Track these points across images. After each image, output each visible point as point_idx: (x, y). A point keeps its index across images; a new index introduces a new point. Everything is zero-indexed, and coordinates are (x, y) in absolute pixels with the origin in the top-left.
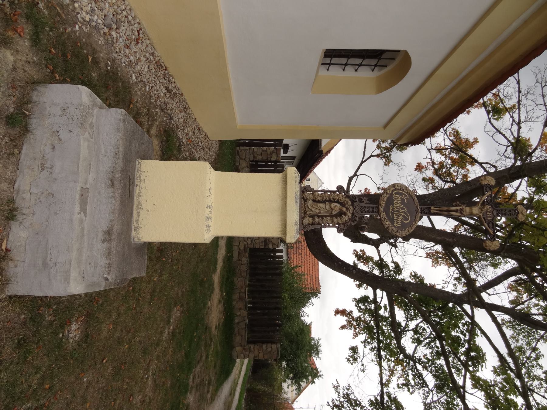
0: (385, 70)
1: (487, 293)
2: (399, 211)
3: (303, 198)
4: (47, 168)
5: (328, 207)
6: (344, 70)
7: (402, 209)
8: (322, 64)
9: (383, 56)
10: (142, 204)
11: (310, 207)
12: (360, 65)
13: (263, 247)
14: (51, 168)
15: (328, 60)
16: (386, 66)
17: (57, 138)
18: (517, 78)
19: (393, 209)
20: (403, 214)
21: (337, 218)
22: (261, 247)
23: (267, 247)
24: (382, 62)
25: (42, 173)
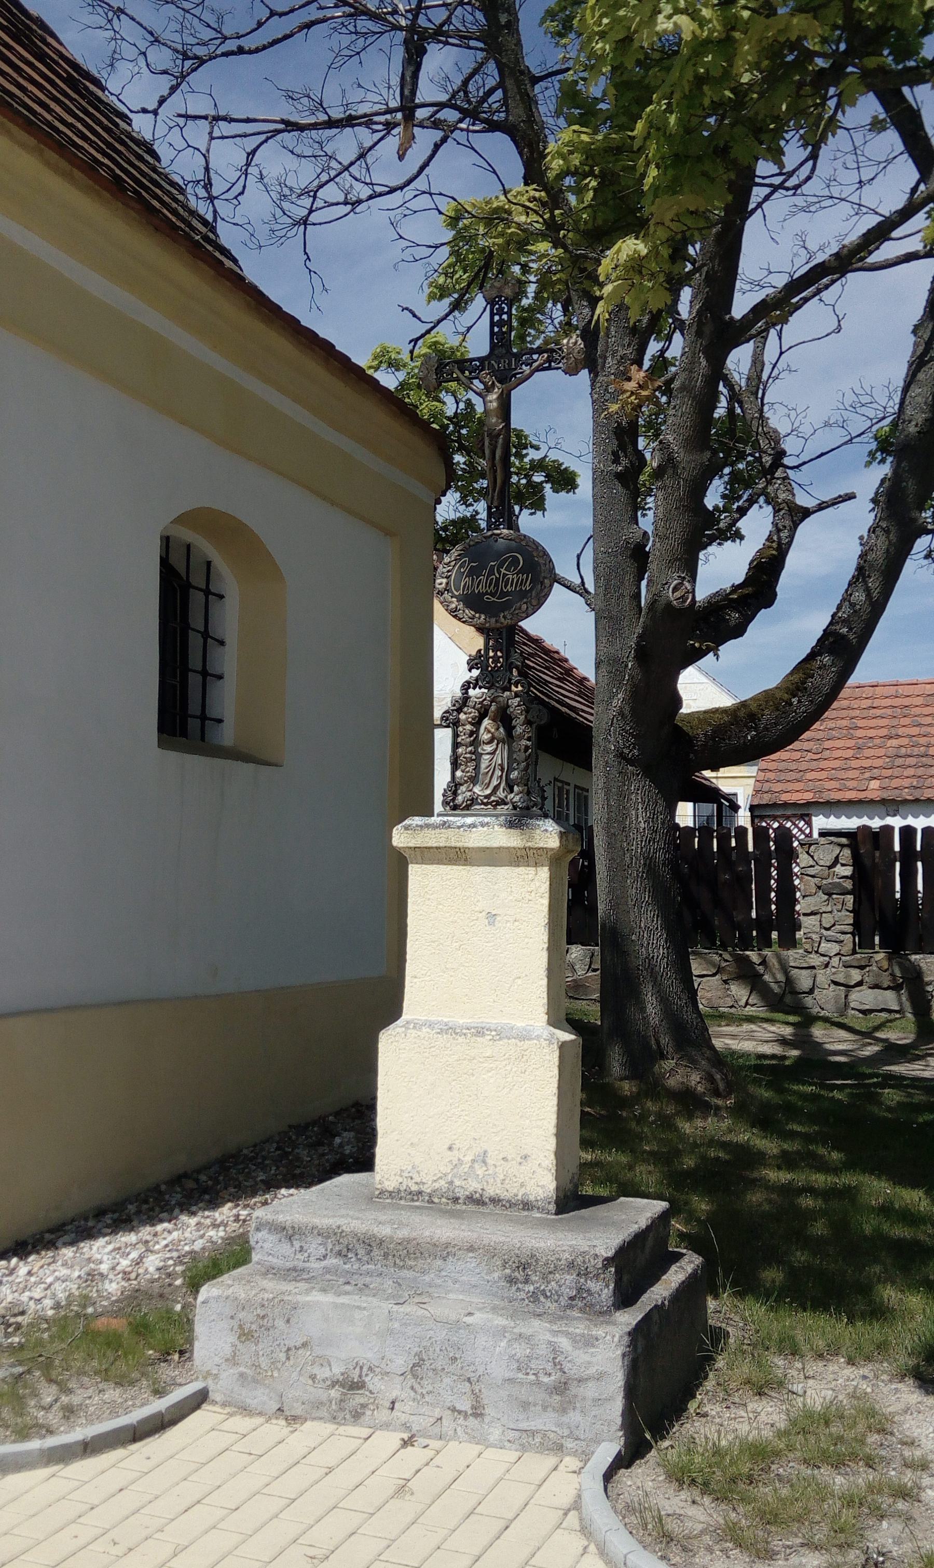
0: (220, 564)
1: (881, 215)
2: (497, 579)
3: (468, 807)
4: (360, 1376)
5: (489, 748)
6: (220, 677)
7: (491, 573)
8: (203, 739)
9: (181, 568)
10: (471, 1189)
11: (488, 792)
12: (206, 635)
13: (850, 899)
14: (361, 1368)
15: (193, 725)
16: (209, 564)
17: (300, 1352)
18: (263, 137)
19: (493, 595)
20: (503, 571)
21: (515, 727)
22: (850, 905)
23: (848, 885)
24: (198, 580)
25: (371, 1387)
